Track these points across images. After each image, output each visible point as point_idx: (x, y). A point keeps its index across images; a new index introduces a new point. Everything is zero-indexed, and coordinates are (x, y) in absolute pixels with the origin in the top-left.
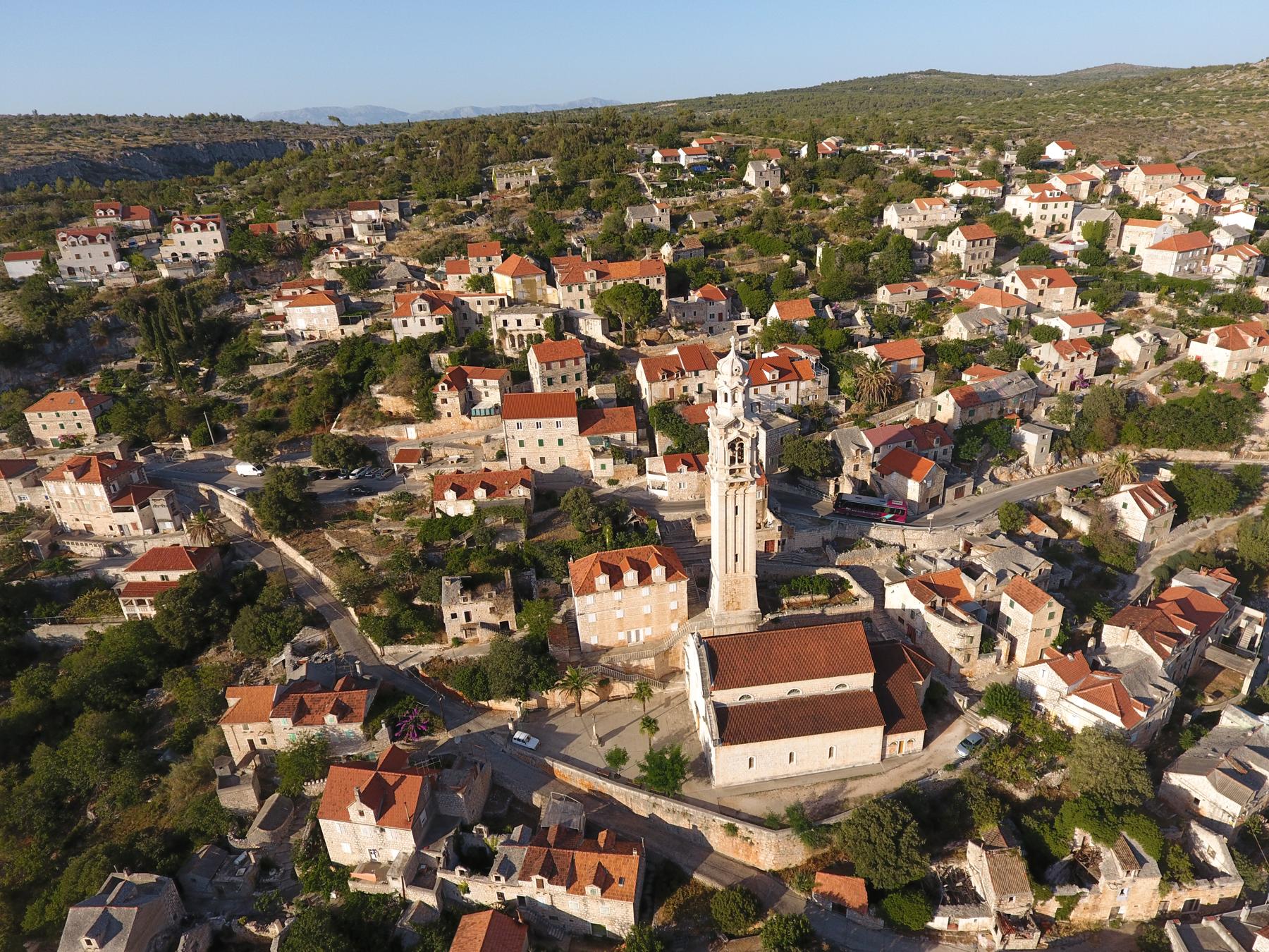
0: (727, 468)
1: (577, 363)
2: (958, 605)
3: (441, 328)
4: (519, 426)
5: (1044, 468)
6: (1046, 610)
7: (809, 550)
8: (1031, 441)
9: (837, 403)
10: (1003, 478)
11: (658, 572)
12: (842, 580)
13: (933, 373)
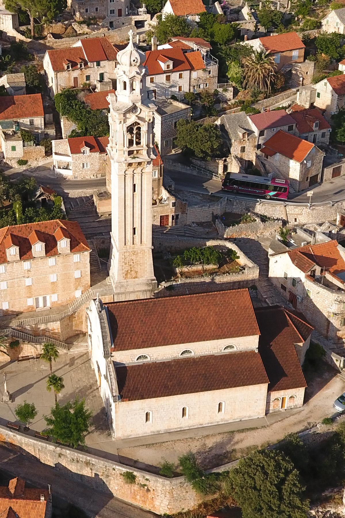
0: (126, 149)
7: (200, 224)
11: (63, 244)
12: (230, 251)
13: (312, 64)
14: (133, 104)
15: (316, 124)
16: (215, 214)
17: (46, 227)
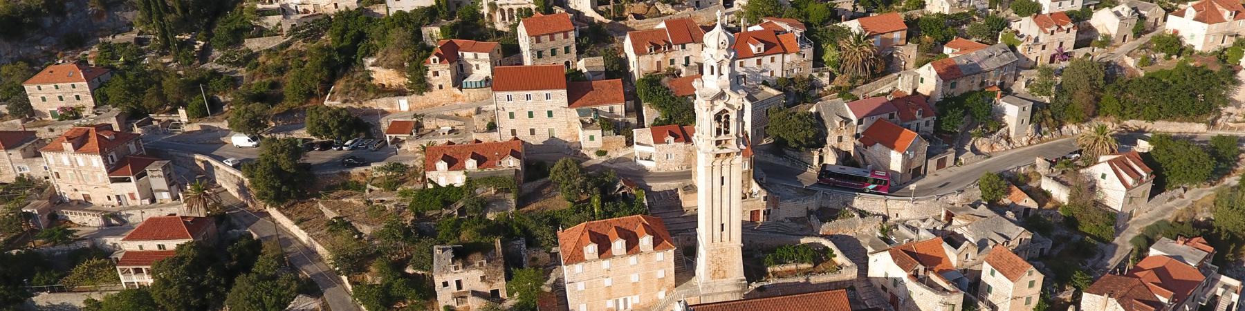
0: (714, 139)
1: (566, 36)
2: (940, 273)
5: (1024, 139)
6: (1026, 279)
7: (794, 220)
8: (1012, 113)
9: (822, 75)
10: (984, 149)
11: (646, 241)
12: (826, 249)
13: (915, 47)
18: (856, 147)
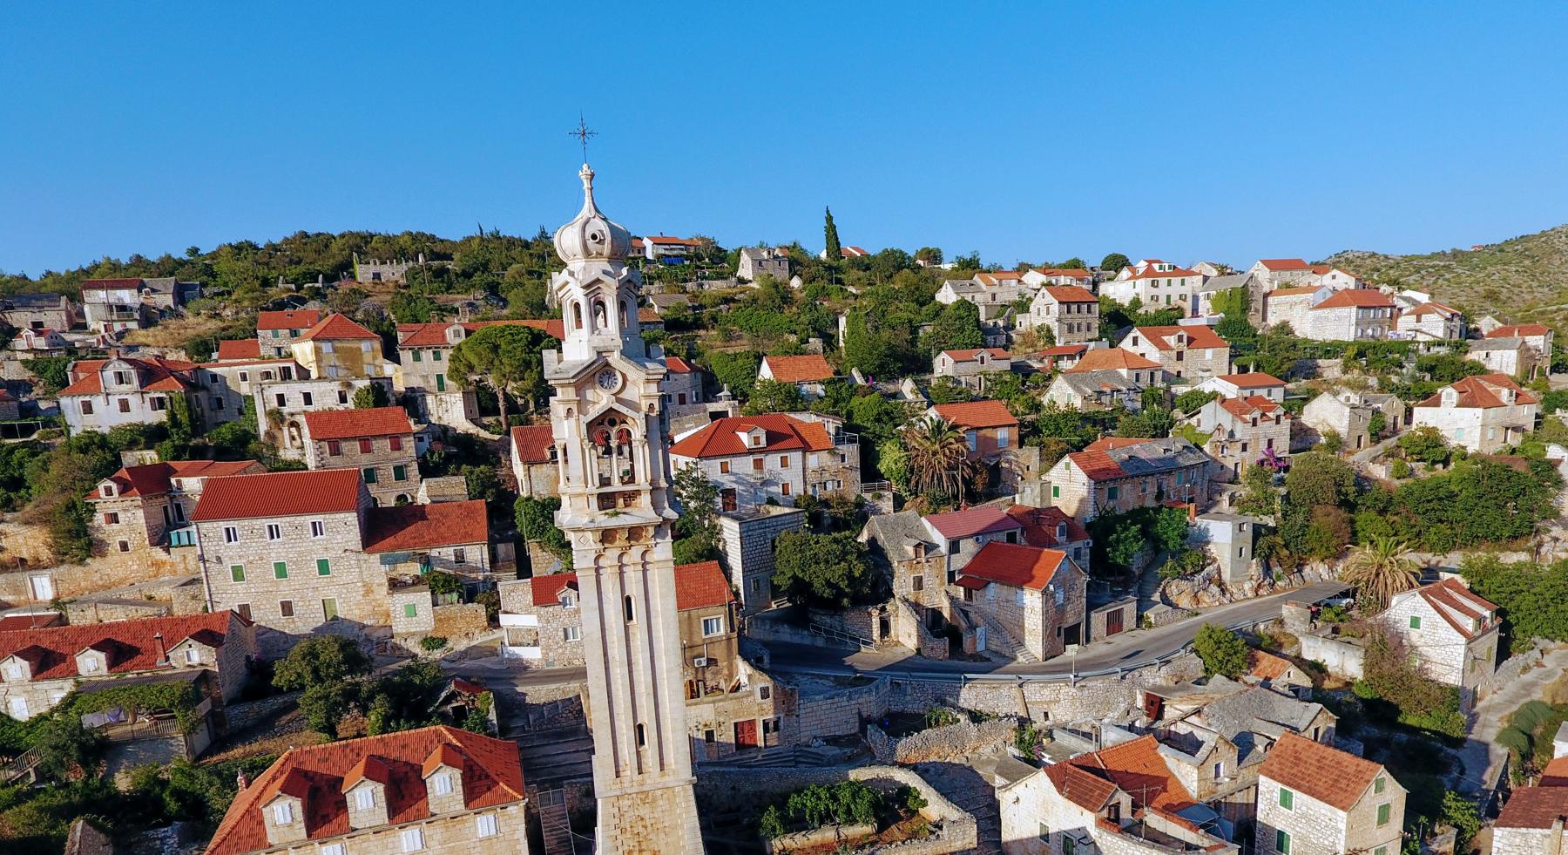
0: (594, 488)
1: (397, 446)
2: (1170, 811)
3: (161, 416)
4: (230, 535)
5: (1247, 586)
6: (1371, 800)
7: (832, 740)
8: (1222, 535)
9: (880, 497)
10: (1185, 602)
11: (443, 784)
12: (905, 791)
13: (1036, 450)
14: (599, 353)
15: (1062, 528)
16: (865, 715)
17: (404, 747)
18: (953, 600)
